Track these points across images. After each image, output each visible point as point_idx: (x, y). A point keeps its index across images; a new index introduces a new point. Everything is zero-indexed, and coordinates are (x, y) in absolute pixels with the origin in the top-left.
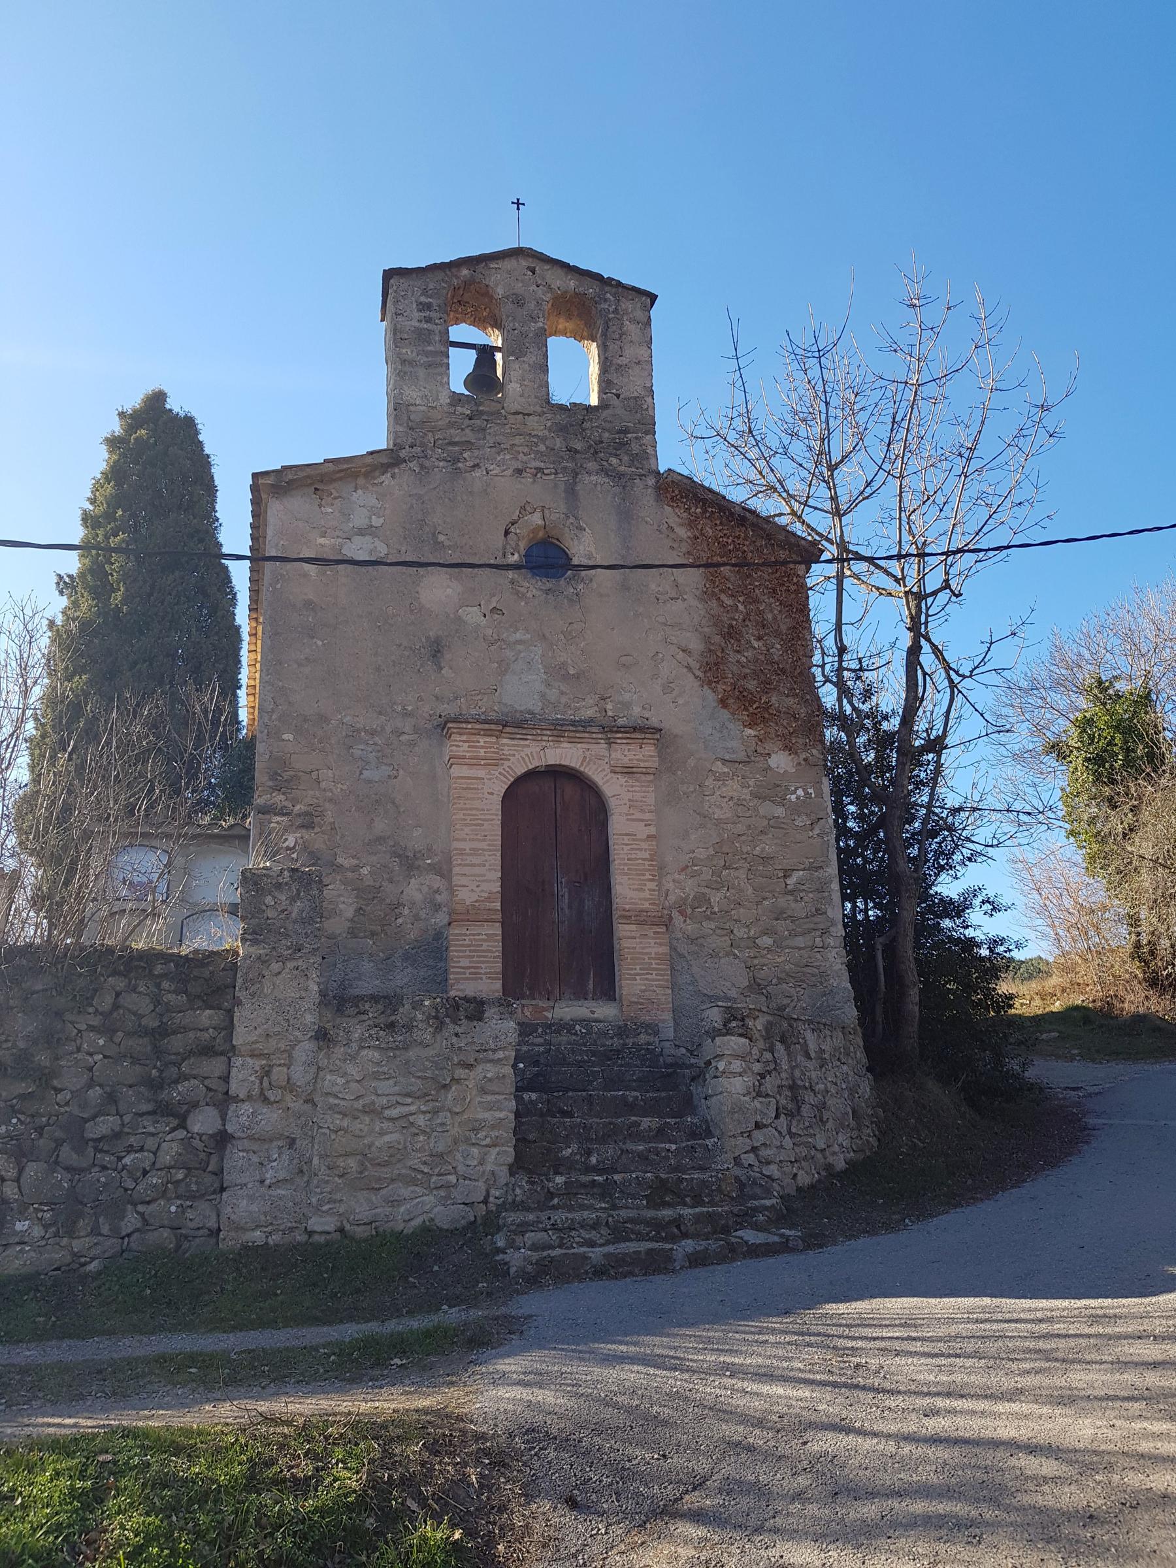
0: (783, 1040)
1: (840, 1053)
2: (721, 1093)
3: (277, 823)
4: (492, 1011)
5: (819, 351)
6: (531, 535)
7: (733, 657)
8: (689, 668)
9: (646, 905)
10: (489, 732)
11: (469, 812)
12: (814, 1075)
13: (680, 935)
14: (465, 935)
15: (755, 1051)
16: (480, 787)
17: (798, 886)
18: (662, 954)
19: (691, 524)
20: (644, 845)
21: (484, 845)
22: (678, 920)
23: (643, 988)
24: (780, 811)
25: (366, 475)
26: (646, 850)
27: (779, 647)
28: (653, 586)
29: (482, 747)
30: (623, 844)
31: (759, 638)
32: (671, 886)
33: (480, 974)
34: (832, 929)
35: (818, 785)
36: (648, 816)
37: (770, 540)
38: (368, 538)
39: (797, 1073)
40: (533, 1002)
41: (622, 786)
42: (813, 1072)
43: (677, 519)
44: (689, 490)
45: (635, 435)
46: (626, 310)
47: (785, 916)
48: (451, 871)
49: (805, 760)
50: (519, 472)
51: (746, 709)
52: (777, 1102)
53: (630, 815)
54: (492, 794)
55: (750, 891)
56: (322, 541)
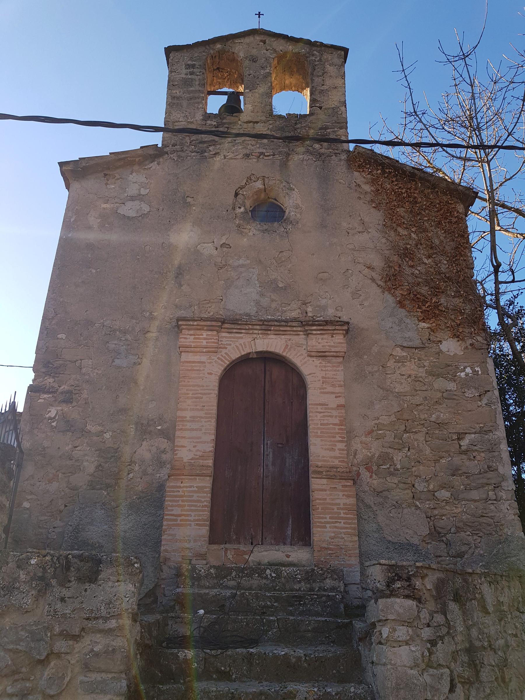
0: (457, 598)
1: (519, 603)
2: (385, 664)
3: (44, 399)
4: (110, 571)
5: (464, 54)
6: (255, 197)
7: (408, 271)
8: (373, 280)
9: (336, 462)
10: (211, 328)
11: (191, 388)
12: (492, 631)
13: (367, 489)
14: (180, 487)
15: (425, 615)
16: (202, 368)
17: (471, 447)
18: (349, 505)
19: (373, 182)
20: (335, 413)
21: (202, 414)
22: (365, 475)
23: (333, 535)
24: (452, 386)
25: (140, 163)
26: (336, 417)
27: (445, 262)
28: (344, 224)
29: (205, 339)
30: (317, 412)
31: (429, 257)
32: (359, 446)
33: (190, 521)
34: (503, 484)
35: (483, 365)
36: (338, 390)
37: (435, 188)
38: (137, 203)
39: (474, 632)
40: (236, 546)
41: (316, 366)
42: (492, 628)
43: (363, 179)
44: (371, 158)
45: (332, 130)
46: (327, 59)
47: (460, 472)
48: (174, 435)
49: (471, 345)
50: (247, 156)
51: (419, 307)
52: (452, 672)
53: (323, 389)
54: (211, 374)
55: (428, 451)
56: (104, 206)
